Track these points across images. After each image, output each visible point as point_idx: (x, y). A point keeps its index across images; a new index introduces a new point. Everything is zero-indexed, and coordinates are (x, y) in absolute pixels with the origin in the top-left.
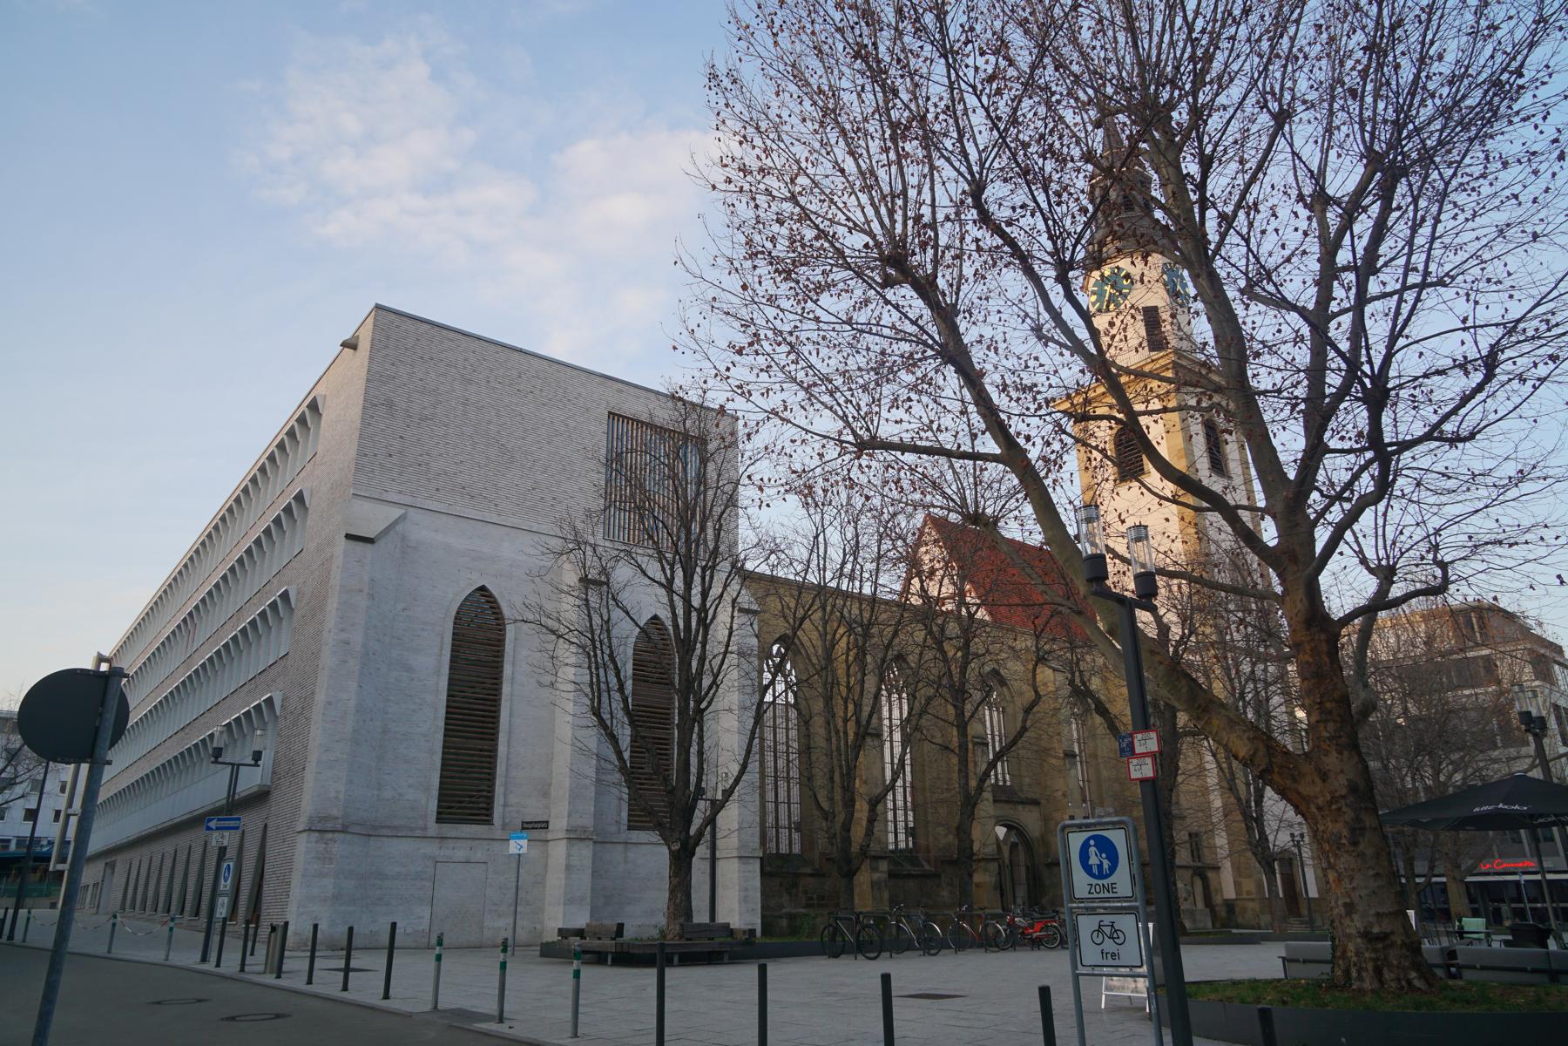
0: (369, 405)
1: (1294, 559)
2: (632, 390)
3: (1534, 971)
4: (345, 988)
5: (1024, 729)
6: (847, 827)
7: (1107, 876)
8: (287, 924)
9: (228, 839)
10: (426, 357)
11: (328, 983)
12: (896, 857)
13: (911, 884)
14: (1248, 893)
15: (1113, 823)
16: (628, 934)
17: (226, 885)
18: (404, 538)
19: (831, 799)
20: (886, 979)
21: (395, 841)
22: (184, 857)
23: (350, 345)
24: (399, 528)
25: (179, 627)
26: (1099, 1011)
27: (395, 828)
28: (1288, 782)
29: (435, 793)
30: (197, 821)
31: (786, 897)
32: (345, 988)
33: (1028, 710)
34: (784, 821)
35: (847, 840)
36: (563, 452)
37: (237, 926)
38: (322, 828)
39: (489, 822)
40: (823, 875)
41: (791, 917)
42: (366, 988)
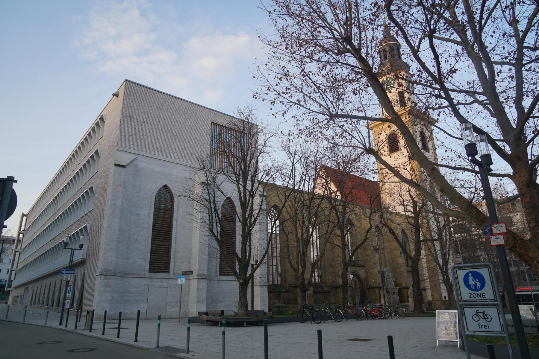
0: (123, 116)
1: (519, 159)
2: (220, 114)
3: (532, 327)
4: (118, 337)
5: (366, 239)
6: (303, 274)
7: (479, 290)
8: (94, 310)
9: (70, 278)
10: (145, 99)
11: (111, 334)
12: (315, 285)
13: (320, 295)
14: (437, 298)
15: (482, 266)
16: (225, 314)
17: (69, 295)
18: (136, 166)
19: (298, 264)
20: (320, 332)
21: (133, 279)
22: (53, 286)
23: (116, 95)
24: (135, 162)
25: (51, 202)
26: (436, 347)
27: (133, 274)
28: (523, 252)
29: (148, 261)
30: (58, 272)
31: (276, 300)
32: (118, 337)
33: (368, 232)
34: (275, 273)
35: (303, 279)
36: (195, 136)
37: (74, 311)
38: (105, 274)
39: (168, 272)
40: (289, 292)
41: (278, 307)
42: (127, 337)
